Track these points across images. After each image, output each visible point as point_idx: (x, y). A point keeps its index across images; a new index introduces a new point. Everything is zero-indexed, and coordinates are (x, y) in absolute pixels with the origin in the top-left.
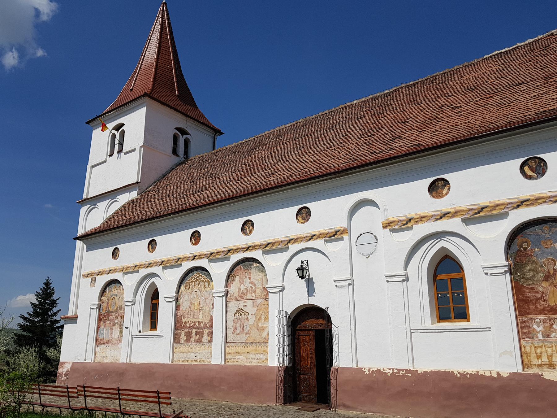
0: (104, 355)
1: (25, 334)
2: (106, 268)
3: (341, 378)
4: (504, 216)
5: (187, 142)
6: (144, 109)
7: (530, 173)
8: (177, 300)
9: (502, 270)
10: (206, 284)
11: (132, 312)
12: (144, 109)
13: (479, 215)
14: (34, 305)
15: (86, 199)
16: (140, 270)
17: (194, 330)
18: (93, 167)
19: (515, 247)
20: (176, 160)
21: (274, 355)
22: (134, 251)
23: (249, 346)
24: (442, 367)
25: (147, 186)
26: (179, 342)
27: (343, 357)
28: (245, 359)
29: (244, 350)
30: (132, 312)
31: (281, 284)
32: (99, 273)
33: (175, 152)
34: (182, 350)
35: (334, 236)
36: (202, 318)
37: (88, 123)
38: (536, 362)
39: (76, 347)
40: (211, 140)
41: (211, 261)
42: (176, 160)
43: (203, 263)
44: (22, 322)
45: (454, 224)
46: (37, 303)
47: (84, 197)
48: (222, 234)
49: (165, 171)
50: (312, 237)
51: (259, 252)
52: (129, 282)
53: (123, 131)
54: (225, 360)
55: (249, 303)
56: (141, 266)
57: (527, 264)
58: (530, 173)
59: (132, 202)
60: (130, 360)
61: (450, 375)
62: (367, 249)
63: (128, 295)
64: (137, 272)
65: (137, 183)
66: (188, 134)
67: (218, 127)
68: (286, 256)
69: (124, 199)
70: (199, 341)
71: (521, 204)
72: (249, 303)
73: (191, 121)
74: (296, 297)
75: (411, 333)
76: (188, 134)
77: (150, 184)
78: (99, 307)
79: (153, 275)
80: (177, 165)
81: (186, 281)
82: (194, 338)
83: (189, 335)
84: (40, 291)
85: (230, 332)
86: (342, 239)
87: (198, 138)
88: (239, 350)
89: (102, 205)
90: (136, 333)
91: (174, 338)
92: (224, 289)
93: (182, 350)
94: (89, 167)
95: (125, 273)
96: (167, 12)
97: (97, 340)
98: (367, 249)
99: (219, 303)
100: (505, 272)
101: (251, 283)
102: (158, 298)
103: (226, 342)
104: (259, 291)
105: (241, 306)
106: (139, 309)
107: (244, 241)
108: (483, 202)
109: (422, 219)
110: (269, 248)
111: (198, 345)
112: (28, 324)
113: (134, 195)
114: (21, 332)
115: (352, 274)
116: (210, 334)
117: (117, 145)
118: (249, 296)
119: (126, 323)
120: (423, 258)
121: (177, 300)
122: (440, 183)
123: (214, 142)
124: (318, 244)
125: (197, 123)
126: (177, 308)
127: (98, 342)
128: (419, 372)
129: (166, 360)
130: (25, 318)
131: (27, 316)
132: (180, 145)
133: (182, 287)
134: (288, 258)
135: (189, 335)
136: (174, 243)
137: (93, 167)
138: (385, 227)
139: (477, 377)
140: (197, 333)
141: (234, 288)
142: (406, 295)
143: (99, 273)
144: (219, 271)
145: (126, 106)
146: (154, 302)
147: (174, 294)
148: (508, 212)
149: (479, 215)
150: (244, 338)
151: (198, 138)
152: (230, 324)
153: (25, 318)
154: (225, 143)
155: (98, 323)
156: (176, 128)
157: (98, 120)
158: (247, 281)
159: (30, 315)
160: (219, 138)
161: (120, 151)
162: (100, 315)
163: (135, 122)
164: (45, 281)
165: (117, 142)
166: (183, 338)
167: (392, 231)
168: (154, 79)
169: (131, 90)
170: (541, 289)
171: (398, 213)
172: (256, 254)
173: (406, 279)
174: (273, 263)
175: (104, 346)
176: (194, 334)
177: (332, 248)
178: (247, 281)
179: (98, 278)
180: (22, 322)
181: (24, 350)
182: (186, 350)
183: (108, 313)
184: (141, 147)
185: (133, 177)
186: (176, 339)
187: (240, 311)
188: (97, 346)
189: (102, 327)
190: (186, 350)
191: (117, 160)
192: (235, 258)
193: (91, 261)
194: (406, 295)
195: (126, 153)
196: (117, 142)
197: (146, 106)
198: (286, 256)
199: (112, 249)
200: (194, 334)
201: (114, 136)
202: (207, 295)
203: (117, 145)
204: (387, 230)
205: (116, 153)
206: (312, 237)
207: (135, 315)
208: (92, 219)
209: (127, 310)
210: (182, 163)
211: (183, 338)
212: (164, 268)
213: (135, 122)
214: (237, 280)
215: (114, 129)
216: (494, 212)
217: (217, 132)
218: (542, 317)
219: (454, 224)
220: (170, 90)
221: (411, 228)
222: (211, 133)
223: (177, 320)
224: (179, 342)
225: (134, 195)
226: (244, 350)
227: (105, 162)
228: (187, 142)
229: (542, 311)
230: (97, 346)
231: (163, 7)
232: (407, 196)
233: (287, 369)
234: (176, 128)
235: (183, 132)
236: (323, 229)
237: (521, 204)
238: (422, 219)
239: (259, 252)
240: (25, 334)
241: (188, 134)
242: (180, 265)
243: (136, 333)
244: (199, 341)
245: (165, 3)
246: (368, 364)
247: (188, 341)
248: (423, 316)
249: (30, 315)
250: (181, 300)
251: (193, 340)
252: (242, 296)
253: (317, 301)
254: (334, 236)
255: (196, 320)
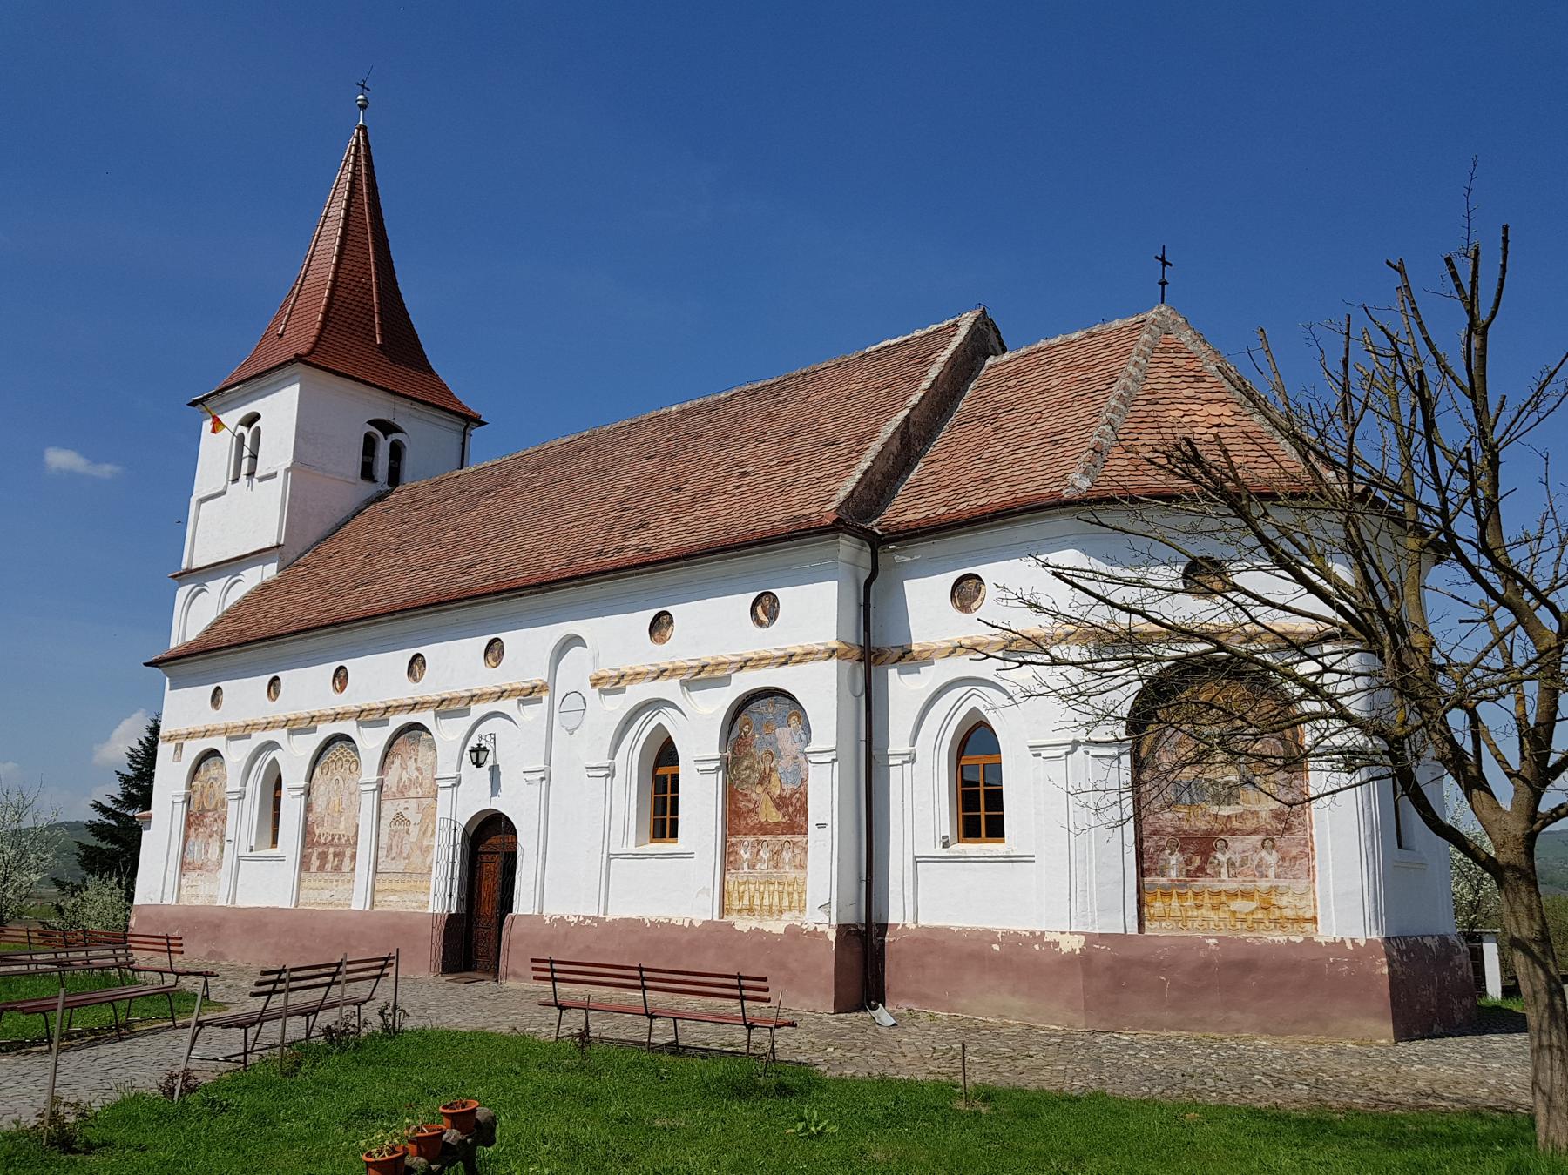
0: (193, 891)
1: (104, 845)
2: (199, 726)
3: (517, 929)
4: (725, 681)
5: (396, 451)
6: (297, 386)
7: (762, 617)
8: (308, 793)
9: (713, 766)
10: (353, 766)
11: (240, 812)
12: (295, 389)
13: (701, 677)
14: (126, 779)
15: (189, 571)
16: (254, 735)
17: (331, 850)
18: (202, 501)
19: (736, 730)
20: (369, 489)
21: (437, 896)
22: (245, 696)
23: (407, 878)
24: (635, 915)
25: (300, 551)
26: (308, 870)
27: (531, 897)
28: (399, 902)
29: (399, 886)
30: (240, 812)
31: (454, 774)
32: (189, 735)
33: (367, 472)
34: (312, 884)
35: (530, 694)
36: (343, 828)
37: (193, 404)
38: (737, 905)
39: (156, 881)
40: (457, 439)
41: (362, 724)
42: (369, 489)
43: (348, 727)
44: (97, 817)
45: (668, 689)
46: (131, 773)
47: (184, 566)
48: (378, 675)
49: (339, 517)
50: (501, 694)
51: (431, 713)
52: (235, 755)
53: (258, 430)
54: (373, 903)
55: (413, 804)
56: (255, 726)
57: (744, 758)
58: (762, 617)
59: (264, 587)
60: (234, 902)
61: (640, 922)
62: (572, 720)
63: (233, 783)
64: (249, 736)
65: (279, 546)
66: (401, 431)
67: (475, 408)
68: (465, 723)
69: (253, 577)
70: (337, 869)
71: (745, 664)
72: (413, 804)
73: (408, 403)
74: (473, 799)
75: (609, 859)
76: (399, 430)
77: (299, 551)
78: (188, 800)
79: (272, 745)
80: (371, 502)
81: (323, 760)
82: (331, 862)
83: (323, 857)
84: (139, 747)
85: (382, 853)
86: (540, 700)
87: (423, 436)
88: (393, 886)
89: (215, 586)
90: (244, 852)
91: (302, 863)
92: (375, 778)
93: (312, 884)
94: (193, 500)
95: (231, 738)
96: (368, 147)
97: (183, 864)
98: (572, 720)
99: (368, 801)
100: (717, 769)
101: (418, 769)
102: (675, 762)
103: (376, 872)
104: (427, 783)
105: (401, 810)
106: (252, 807)
107: (410, 691)
108: (706, 658)
109: (636, 676)
110: (447, 707)
111: (336, 877)
112: (113, 823)
113: (270, 571)
114: (93, 841)
115: (548, 762)
116: (353, 857)
117: (246, 461)
118: (413, 793)
119: (229, 835)
120: (636, 739)
121: (308, 793)
122: (665, 619)
123: (463, 444)
124: (508, 705)
125: (420, 407)
126: (308, 808)
127: (184, 866)
128: (697, 925)
129: (284, 901)
130: (104, 810)
131: (108, 804)
132: (381, 461)
133: (318, 770)
134: (468, 728)
135: (323, 857)
136: (307, 687)
137: (202, 501)
138: (594, 685)
139: (669, 926)
140: (335, 855)
141: (391, 779)
142: (609, 796)
143: (189, 735)
144: (371, 742)
145: (260, 379)
146: (661, 771)
147: (303, 783)
148: (729, 677)
149: (701, 677)
150: (401, 865)
151: (423, 436)
152: (384, 840)
153: (104, 810)
154: (485, 451)
155: (186, 832)
156: (370, 422)
157: (208, 403)
158: (411, 764)
159: (115, 801)
160: (476, 432)
161: (251, 474)
162: (188, 815)
163: (280, 409)
164: (151, 725)
165: (246, 452)
166: (315, 862)
167: (604, 692)
168: (325, 315)
169: (281, 336)
170: (754, 796)
171: (609, 666)
172: (425, 717)
173: (611, 774)
174: (449, 734)
175: (194, 874)
176: (331, 857)
177: (533, 715)
178: (411, 764)
179: (186, 743)
180: (97, 817)
181: (93, 881)
182: (317, 884)
183: (203, 812)
184: (287, 470)
185: (269, 535)
186: (304, 864)
187: (399, 818)
188: (182, 874)
189: (192, 839)
190: (317, 884)
191: (241, 500)
192: (398, 721)
193: (184, 708)
194: (609, 796)
195: (261, 479)
196: (246, 452)
197: (300, 381)
198: (467, 722)
199: (212, 688)
200: (331, 857)
201: (241, 438)
202: (352, 789)
203: (246, 461)
204: (596, 690)
205: (243, 478)
206: (501, 694)
207: (243, 817)
208: (195, 615)
209: (232, 806)
210: (380, 498)
211: (315, 862)
212: (292, 732)
213: (280, 409)
214: (398, 762)
215: (241, 423)
216: (716, 674)
217: (471, 420)
218: (751, 838)
219: (668, 689)
220: (368, 334)
221: (623, 690)
222: (458, 425)
223: (307, 830)
224: (308, 870)
225: (270, 571)
226: (399, 886)
227: (224, 493)
228: (396, 451)
229: (751, 830)
230: (182, 874)
231: (357, 146)
232: (614, 636)
233: (452, 918)
234: (370, 422)
235: (387, 427)
236: (518, 682)
237: (745, 664)
238: (636, 676)
239: (431, 713)
240: (104, 845)
241: (401, 431)
242: (314, 730)
243: (244, 852)
244: (337, 869)
245: (364, 128)
246: (552, 910)
247: (321, 868)
248: (626, 833)
249: (115, 801)
250: (314, 794)
251: (328, 867)
252: (402, 792)
253: (501, 805)
254: (530, 694)
255: (335, 831)
